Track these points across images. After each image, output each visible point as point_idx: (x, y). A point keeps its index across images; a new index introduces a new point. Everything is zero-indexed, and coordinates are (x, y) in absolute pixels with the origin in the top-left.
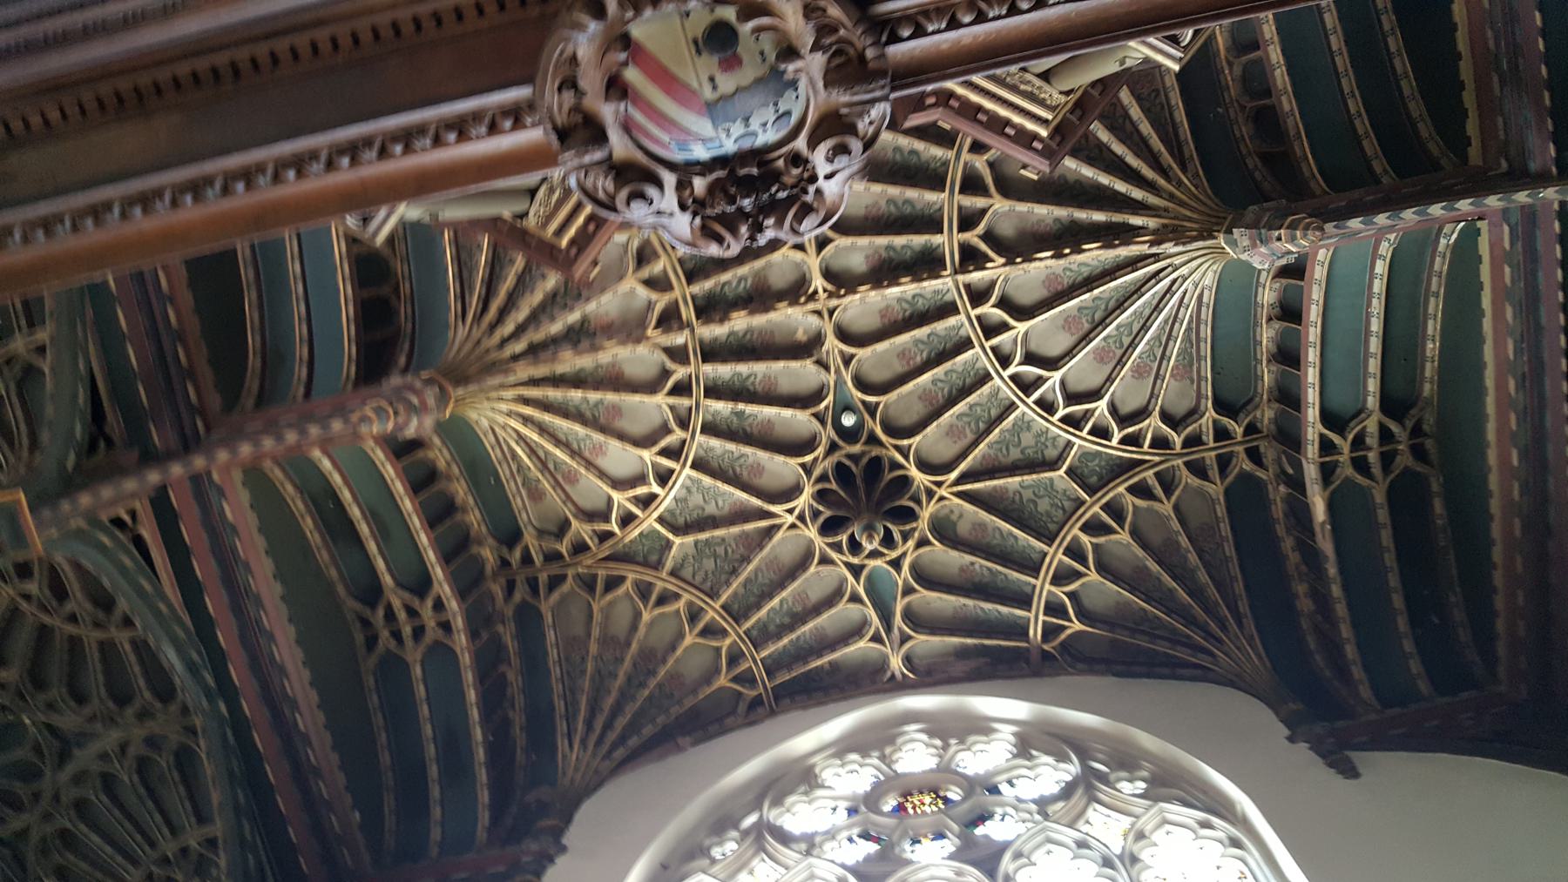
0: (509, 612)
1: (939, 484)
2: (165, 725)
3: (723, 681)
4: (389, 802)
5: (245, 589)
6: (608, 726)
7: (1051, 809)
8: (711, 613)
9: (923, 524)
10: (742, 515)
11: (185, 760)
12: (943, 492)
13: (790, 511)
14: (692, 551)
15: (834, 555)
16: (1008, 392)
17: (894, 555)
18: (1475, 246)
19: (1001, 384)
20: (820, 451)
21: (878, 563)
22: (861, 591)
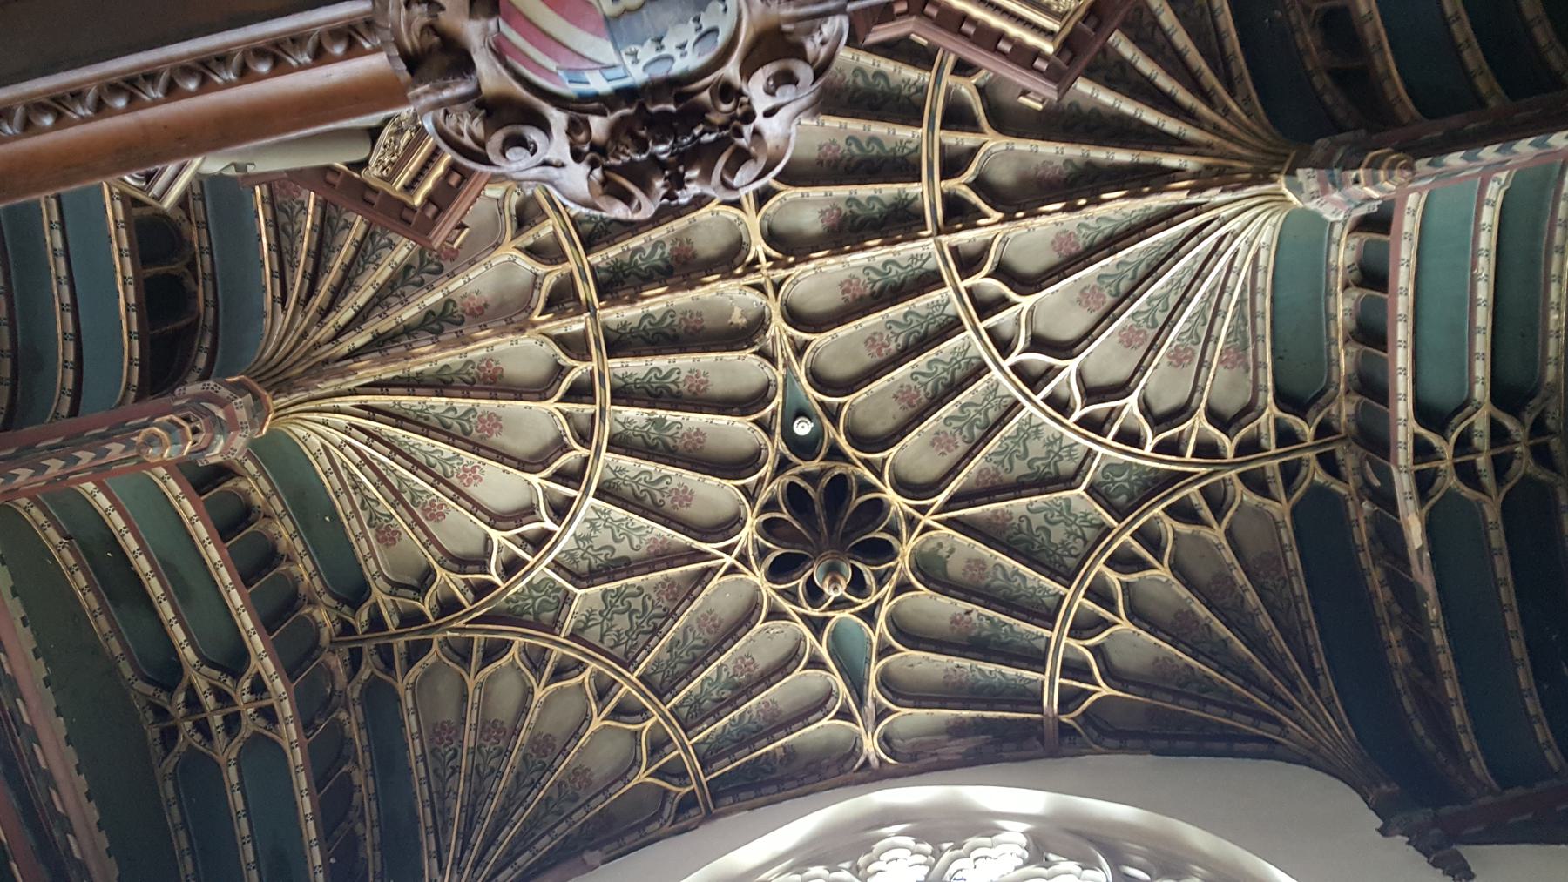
6: (490, 841)
9: (903, 563)
15: (787, 606)
19: (1000, 379)
20: (767, 470)
21: (846, 614)
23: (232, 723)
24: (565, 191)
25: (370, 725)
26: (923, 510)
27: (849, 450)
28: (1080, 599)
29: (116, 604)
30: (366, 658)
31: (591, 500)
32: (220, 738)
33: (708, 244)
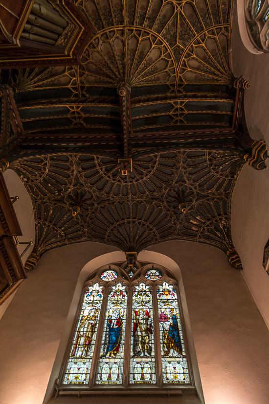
2: (181, 158)
3: (69, 86)
6: (219, 70)
7: (119, 32)
10: (175, 24)
11: (190, 156)
14: (182, 41)
23: (182, 109)
24: (58, 13)
33: (189, 11)
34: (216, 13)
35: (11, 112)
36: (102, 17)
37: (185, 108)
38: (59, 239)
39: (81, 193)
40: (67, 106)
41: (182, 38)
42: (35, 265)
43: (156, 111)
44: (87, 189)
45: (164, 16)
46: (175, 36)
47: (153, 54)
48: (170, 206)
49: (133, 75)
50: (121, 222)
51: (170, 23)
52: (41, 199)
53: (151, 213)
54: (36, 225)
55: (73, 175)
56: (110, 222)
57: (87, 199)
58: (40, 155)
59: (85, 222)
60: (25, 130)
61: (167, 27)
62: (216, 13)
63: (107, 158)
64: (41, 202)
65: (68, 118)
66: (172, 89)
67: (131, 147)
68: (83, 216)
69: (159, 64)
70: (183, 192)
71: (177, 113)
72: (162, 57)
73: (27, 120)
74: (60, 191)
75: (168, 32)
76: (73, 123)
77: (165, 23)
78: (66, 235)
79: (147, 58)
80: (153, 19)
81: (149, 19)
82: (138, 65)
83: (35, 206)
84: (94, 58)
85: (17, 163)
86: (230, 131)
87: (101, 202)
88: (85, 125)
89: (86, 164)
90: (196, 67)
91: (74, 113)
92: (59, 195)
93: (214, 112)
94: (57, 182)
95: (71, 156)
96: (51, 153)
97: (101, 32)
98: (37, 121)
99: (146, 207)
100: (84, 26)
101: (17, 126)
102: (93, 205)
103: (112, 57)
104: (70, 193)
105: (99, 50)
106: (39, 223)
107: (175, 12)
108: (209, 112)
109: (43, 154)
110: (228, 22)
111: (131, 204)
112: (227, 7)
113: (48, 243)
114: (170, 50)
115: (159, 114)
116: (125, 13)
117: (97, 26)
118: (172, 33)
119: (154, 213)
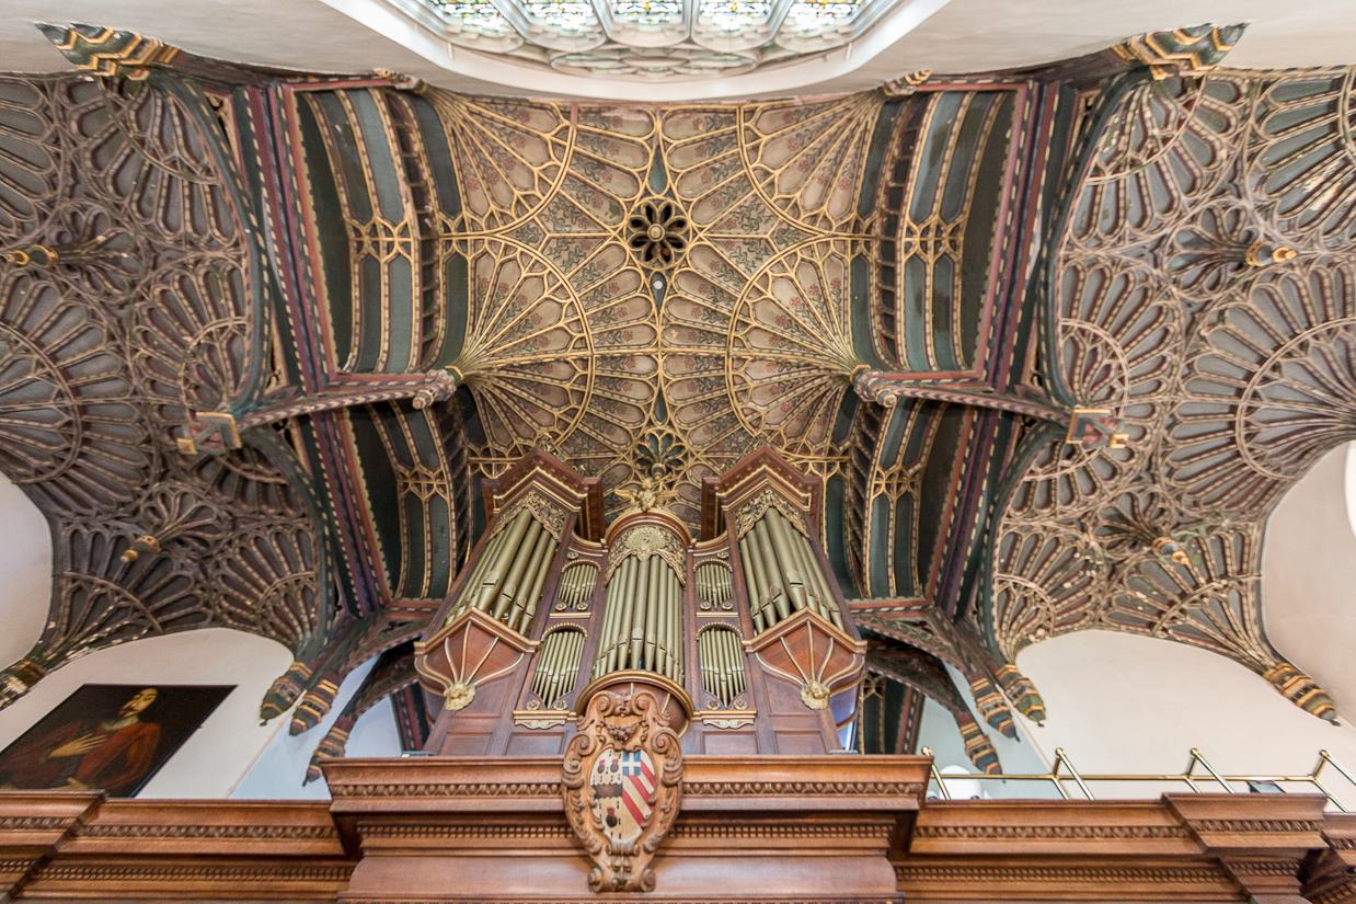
0: (876, 214)
1: (615, 238)
2: (1084, 251)
4: (988, 126)
5: (976, 562)
8: (760, 186)
9: (628, 216)
10: (728, 243)
12: (614, 234)
13: (700, 239)
14: (761, 225)
15: (681, 206)
16: (571, 289)
17: (647, 199)
18: (340, 357)
19: (585, 406)
20: (676, 272)
21: (656, 196)
22: (670, 181)
25: (874, 197)
26: (615, 238)
27: (641, 272)
28: (554, 185)
29: (948, 299)
30: (865, 229)
31: (750, 279)
32: (933, 226)
34: (714, 144)
35: (879, 614)
36: (708, 396)
37: (923, 222)
38: (1233, 596)
39: (1110, 518)
40: (873, 497)
41: (754, 226)
42: (1315, 687)
43: (919, 299)
44: (1104, 504)
45: (713, 266)
46: (750, 243)
47: (783, 294)
48: (1233, 282)
49: (824, 347)
50: (1241, 432)
51: (726, 255)
52: (1095, 609)
53: (1242, 341)
54: (1170, 638)
55: (1056, 531)
56: (1224, 446)
57: (1133, 507)
58: (992, 593)
59: (1199, 521)
60: (912, 594)
61: (732, 262)
62: (714, 144)
63: (1042, 454)
64: (1105, 609)
65: (899, 500)
66: (861, 248)
67: (1017, 387)
68: (1179, 524)
69: (806, 280)
70: (1198, 241)
71: (931, 244)
72: (792, 275)
73: (892, 582)
74: (1087, 565)
75: (742, 258)
76: (910, 490)
77: (726, 264)
78: (1225, 575)
79: (792, 312)
80: (717, 292)
81: (715, 301)
82: (805, 332)
83: (1109, 626)
84: (776, 420)
85: (1005, 644)
86: (1029, 96)
87: (1153, 476)
88: (918, 467)
89: (1038, 496)
90: (820, 187)
91: (888, 486)
92: (1098, 570)
93: (952, 141)
94: (1063, 566)
95: (1006, 526)
96: (991, 569)
97: (734, 403)
98: (895, 563)
99: (1214, 356)
100: (760, 465)
101: (907, 609)
102: (1152, 496)
103: (783, 387)
104: (1101, 545)
105: (763, 408)
106: (1164, 630)
107: (709, 243)
108: (948, 155)
109: (990, 586)
110: (734, 112)
111: (1186, 398)
112: (703, 116)
113: (1238, 626)
114: (780, 253)
115: (929, 293)
116: (703, 351)
117: (720, 407)
118: (745, 249)
119: (1240, 332)
